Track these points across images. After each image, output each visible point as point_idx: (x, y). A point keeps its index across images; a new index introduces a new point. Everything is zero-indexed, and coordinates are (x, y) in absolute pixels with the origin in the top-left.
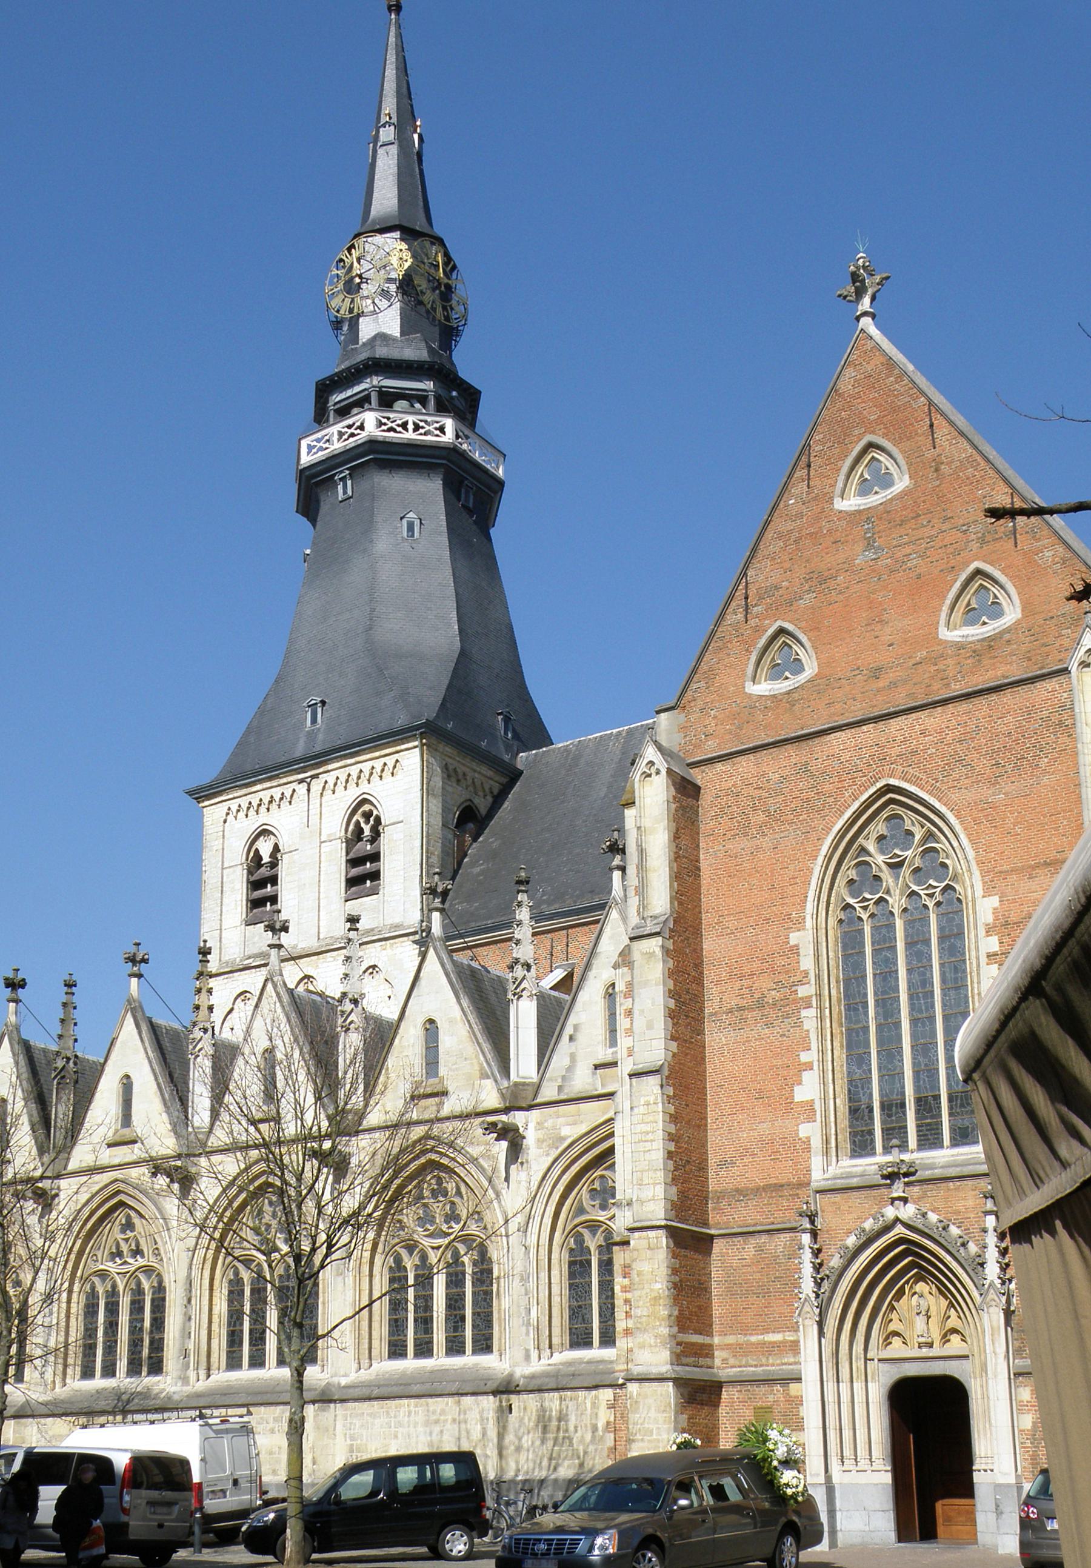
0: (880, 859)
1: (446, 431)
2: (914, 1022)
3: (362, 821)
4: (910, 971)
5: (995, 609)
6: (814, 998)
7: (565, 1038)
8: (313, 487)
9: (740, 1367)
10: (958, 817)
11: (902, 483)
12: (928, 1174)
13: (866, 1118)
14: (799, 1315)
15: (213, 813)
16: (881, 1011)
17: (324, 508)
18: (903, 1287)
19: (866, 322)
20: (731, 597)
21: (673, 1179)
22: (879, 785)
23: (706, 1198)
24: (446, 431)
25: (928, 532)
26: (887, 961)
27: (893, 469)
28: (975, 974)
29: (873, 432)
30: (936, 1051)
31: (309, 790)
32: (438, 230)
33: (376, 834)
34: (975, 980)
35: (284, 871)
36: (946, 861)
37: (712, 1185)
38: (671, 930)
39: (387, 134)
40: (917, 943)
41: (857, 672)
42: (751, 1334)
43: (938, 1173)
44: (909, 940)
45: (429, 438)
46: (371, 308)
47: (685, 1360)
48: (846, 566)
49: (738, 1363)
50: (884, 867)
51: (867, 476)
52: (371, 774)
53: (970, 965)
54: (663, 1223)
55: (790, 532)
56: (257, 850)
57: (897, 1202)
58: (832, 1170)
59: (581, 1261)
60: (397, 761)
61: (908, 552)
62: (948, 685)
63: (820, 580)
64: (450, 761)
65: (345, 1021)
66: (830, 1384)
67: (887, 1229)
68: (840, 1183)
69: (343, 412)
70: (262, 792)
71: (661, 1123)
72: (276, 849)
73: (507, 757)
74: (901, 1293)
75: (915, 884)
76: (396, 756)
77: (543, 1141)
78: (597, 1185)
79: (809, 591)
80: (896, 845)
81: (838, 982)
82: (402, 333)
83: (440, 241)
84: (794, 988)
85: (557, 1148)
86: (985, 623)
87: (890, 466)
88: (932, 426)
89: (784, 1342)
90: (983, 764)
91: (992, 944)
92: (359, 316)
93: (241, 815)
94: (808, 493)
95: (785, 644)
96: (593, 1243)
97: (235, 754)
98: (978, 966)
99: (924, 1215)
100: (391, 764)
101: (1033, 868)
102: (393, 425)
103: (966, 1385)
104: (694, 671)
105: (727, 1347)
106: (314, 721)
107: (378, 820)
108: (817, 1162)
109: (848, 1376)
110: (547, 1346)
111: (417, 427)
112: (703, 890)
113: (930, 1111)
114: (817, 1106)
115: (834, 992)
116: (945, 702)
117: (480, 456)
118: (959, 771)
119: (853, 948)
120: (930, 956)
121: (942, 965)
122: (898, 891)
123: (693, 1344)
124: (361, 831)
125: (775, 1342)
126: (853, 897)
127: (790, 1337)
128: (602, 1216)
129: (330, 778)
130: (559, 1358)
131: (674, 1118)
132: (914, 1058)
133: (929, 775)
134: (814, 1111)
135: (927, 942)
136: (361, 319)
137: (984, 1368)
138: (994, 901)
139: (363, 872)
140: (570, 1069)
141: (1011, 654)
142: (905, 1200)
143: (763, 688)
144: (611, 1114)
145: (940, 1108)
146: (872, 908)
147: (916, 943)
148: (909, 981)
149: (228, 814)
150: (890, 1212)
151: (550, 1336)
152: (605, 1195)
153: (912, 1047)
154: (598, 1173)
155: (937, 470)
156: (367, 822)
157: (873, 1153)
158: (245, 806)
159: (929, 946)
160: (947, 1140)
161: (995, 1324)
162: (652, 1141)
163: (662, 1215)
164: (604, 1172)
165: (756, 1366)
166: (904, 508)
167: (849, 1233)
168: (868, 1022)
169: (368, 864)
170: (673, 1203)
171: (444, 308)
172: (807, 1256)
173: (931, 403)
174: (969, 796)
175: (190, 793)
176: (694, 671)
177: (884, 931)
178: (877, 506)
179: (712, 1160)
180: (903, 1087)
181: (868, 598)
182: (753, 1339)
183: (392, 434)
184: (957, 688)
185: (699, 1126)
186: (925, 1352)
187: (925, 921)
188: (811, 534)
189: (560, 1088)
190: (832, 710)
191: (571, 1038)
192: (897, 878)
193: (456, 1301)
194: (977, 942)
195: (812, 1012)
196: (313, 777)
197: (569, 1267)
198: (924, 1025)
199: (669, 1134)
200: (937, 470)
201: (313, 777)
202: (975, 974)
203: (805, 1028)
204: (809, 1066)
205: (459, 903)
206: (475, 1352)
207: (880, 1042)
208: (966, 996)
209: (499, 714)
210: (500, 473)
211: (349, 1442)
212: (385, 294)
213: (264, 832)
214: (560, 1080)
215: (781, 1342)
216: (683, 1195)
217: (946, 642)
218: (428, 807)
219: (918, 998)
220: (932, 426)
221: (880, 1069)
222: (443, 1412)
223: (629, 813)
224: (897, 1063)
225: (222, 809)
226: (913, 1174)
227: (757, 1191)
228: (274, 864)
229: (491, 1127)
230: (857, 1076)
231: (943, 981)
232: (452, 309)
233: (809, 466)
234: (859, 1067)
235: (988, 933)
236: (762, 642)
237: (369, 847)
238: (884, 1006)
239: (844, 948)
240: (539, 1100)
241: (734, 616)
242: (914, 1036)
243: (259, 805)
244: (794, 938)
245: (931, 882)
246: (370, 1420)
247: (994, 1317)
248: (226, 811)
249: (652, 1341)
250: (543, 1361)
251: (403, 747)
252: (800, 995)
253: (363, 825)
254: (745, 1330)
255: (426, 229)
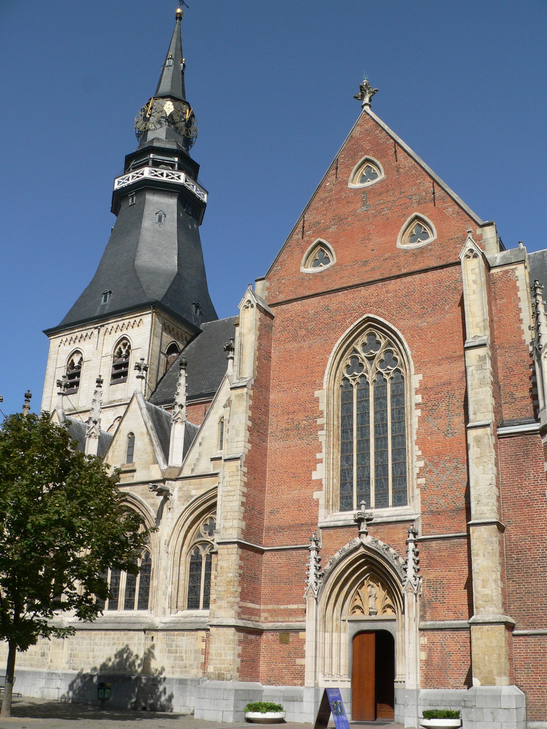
0: (363, 355)
1: (181, 178)
2: (376, 439)
3: (122, 347)
4: (375, 413)
5: (425, 236)
6: (325, 425)
7: (197, 444)
8: (120, 197)
9: (274, 622)
10: (403, 334)
11: (381, 176)
12: (379, 520)
13: (349, 490)
14: (306, 594)
15: (55, 342)
16: (360, 433)
17: (123, 208)
18: (363, 582)
19: (367, 108)
20: (296, 227)
21: (244, 517)
22: (364, 317)
23: (262, 530)
24: (181, 178)
25: (393, 198)
26: (364, 407)
27: (377, 171)
28: (409, 415)
29: (368, 154)
30: (387, 455)
31: (99, 332)
32: (187, 100)
33: (128, 353)
34: (409, 418)
35: (83, 371)
36: (397, 357)
37: (266, 523)
38: (252, 385)
39: (169, 62)
40: (380, 399)
41: (356, 263)
42: (281, 605)
43: (385, 520)
44: (376, 397)
45: (173, 180)
46: (153, 128)
47: (243, 616)
48: (353, 213)
49: (273, 620)
50: (365, 359)
51: (364, 174)
52: (128, 325)
53: (407, 411)
54: (236, 540)
55: (326, 197)
56: (72, 361)
57: (362, 535)
58: (328, 519)
59: (197, 563)
60: (141, 320)
61: (383, 207)
62: (400, 270)
63: (340, 220)
64: (166, 321)
65: (89, 432)
66: (321, 633)
67: (356, 549)
68: (332, 524)
69: (135, 168)
70: (78, 333)
71: (239, 486)
72: (81, 359)
73: (195, 324)
74: (362, 584)
75: (380, 368)
76: (141, 317)
77: (181, 498)
78: (208, 522)
79: (334, 225)
80: (371, 348)
81: (338, 417)
82: (166, 138)
83: (188, 104)
84: (315, 420)
85: (188, 501)
86: (419, 242)
87: (375, 170)
88: (396, 152)
89: (298, 609)
90: (417, 308)
91: (418, 399)
92: (148, 130)
93: (67, 343)
94: (336, 180)
95: (322, 250)
96: (203, 553)
97: (67, 315)
98: (411, 410)
99: (376, 542)
100: (138, 321)
101: (440, 360)
102: (157, 174)
103: (394, 635)
104: (276, 261)
105: (268, 611)
106: (105, 301)
107: (129, 347)
108: (322, 512)
109: (331, 629)
110: (175, 607)
111: (167, 176)
112: (272, 368)
113: (383, 487)
114: (324, 482)
115: (336, 423)
116: (398, 277)
117: (196, 190)
118: (405, 310)
119: (347, 400)
120: (386, 405)
121: (392, 410)
122: (371, 372)
123: (248, 608)
124: (121, 352)
125: (293, 609)
126: (348, 374)
127: (301, 606)
128: (209, 539)
129: (109, 327)
130: (180, 613)
131: (247, 485)
132: (375, 459)
133: (389, 313)
134: (321, 485)
135: (385, 398)
136: (149, 132)
137: (403, 626)
138: (420, 377)
139: (120, 373)
140: (198, 460)
141: (432, 256)
142: (366, 533)
143: (311, 270)
144: (217, 485)
145: (388, 485)
146: (358, 380)
147: (380, 398)
148: (375, 418)
149: (61, 343)
150: (358, 541)
151: (177, 602)
152: (211, 529)
153: (375, 452)
154: (209, 516)
155: (398, 171)
156: (125, 347)
157: (351, 509)
158: (69, 339)
159: (386, 400)
160: (390, 503)
161: (410, 601)
162: (234, 495)
163: (236, 536)
164: (212, 516)
165: (282, 622)
166: (382, 187)
167: (336, 551)
168: (352, 439)
169: (123, 368)
170: (243, 530)
171: (187, 130)
172: (313, 562)
173: (396, 142)
174: (410, 323)
175: (45, 332)
176: (276, 261)
177: (363, 392)
178: (369, 186)
179: (267, 510)
180: (369, 474)
181: (363, 228)
182: (282, 607)
183: (156, 177)
184: (404, 271)
185: (261, 491)
186: (373, 617)
187: (385, 387)
188: (336, 199)
189: (193, 470)
190: (343, 281)
191: (200, 444)
192: (371, 365)
193: (132, 581)
194: (411, 398)
195: (324, 432)
196: (101, 326)
197: (190, 566)
198: (381, 442)
199: (243, 493)
200: (398, 171)
201: (101, 326)
202: (409, 415)
203: (320, 440)
204: (321, 461)
205: (164, 389)
206: (139, 608)
207: (358, 450)
208: (404, 426)
209: (193, 304)
210: (205, 199)
211: (70, 652)
212: (159, 122)
213: (77, 352)
214: (193, 466)
215: (296, 609)
216: (248, 526)
217: (400, 249)
218: (153, 341)
219: (379, 427)
220: (396, 152)
221: (358, 464)
222: (118, 639)
223: (237, 329)
224: (366, 461)
225: (59, 340)
226: (371, 520)
227: (290, 527)
228: (79, 367)
229: (154, 489)
230: (346, 467)
231: (393, 418)
232: (190, 131)
233: (337, 168)
234: (347, 463)
235: (417, 393)
236: (310, 248)
237: (124, 360)
238: (362, 431)
239: (342, 400)
240: (181, 476)
241: (297, 236)
242: (376, 447)
243: (76, 339)
244: (317, 393)
245: (389, 367)
246: (81, 641)
247: (410, 598)
248: (60, 341)
249: (226, 605)
250: (172, 615)
251: (144, 313)
252: (318, 423)
253: (122, 349)
254: (278, 602)
255: (183, 99)
